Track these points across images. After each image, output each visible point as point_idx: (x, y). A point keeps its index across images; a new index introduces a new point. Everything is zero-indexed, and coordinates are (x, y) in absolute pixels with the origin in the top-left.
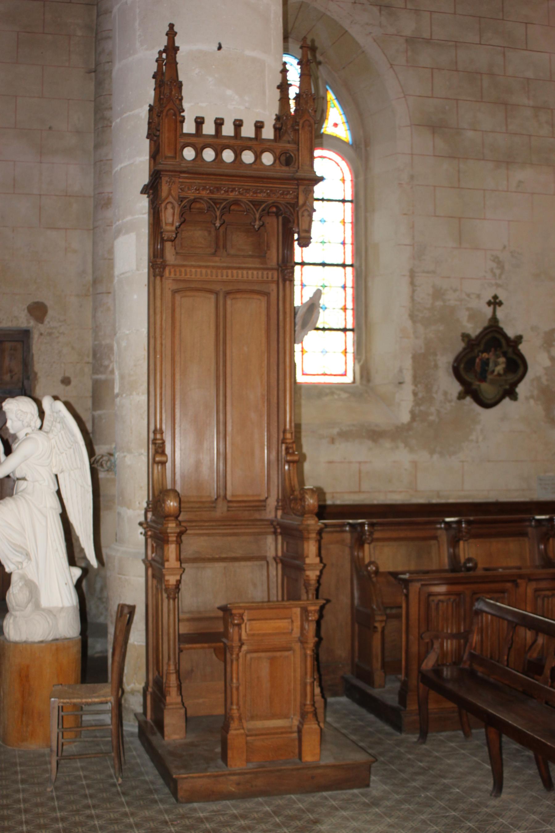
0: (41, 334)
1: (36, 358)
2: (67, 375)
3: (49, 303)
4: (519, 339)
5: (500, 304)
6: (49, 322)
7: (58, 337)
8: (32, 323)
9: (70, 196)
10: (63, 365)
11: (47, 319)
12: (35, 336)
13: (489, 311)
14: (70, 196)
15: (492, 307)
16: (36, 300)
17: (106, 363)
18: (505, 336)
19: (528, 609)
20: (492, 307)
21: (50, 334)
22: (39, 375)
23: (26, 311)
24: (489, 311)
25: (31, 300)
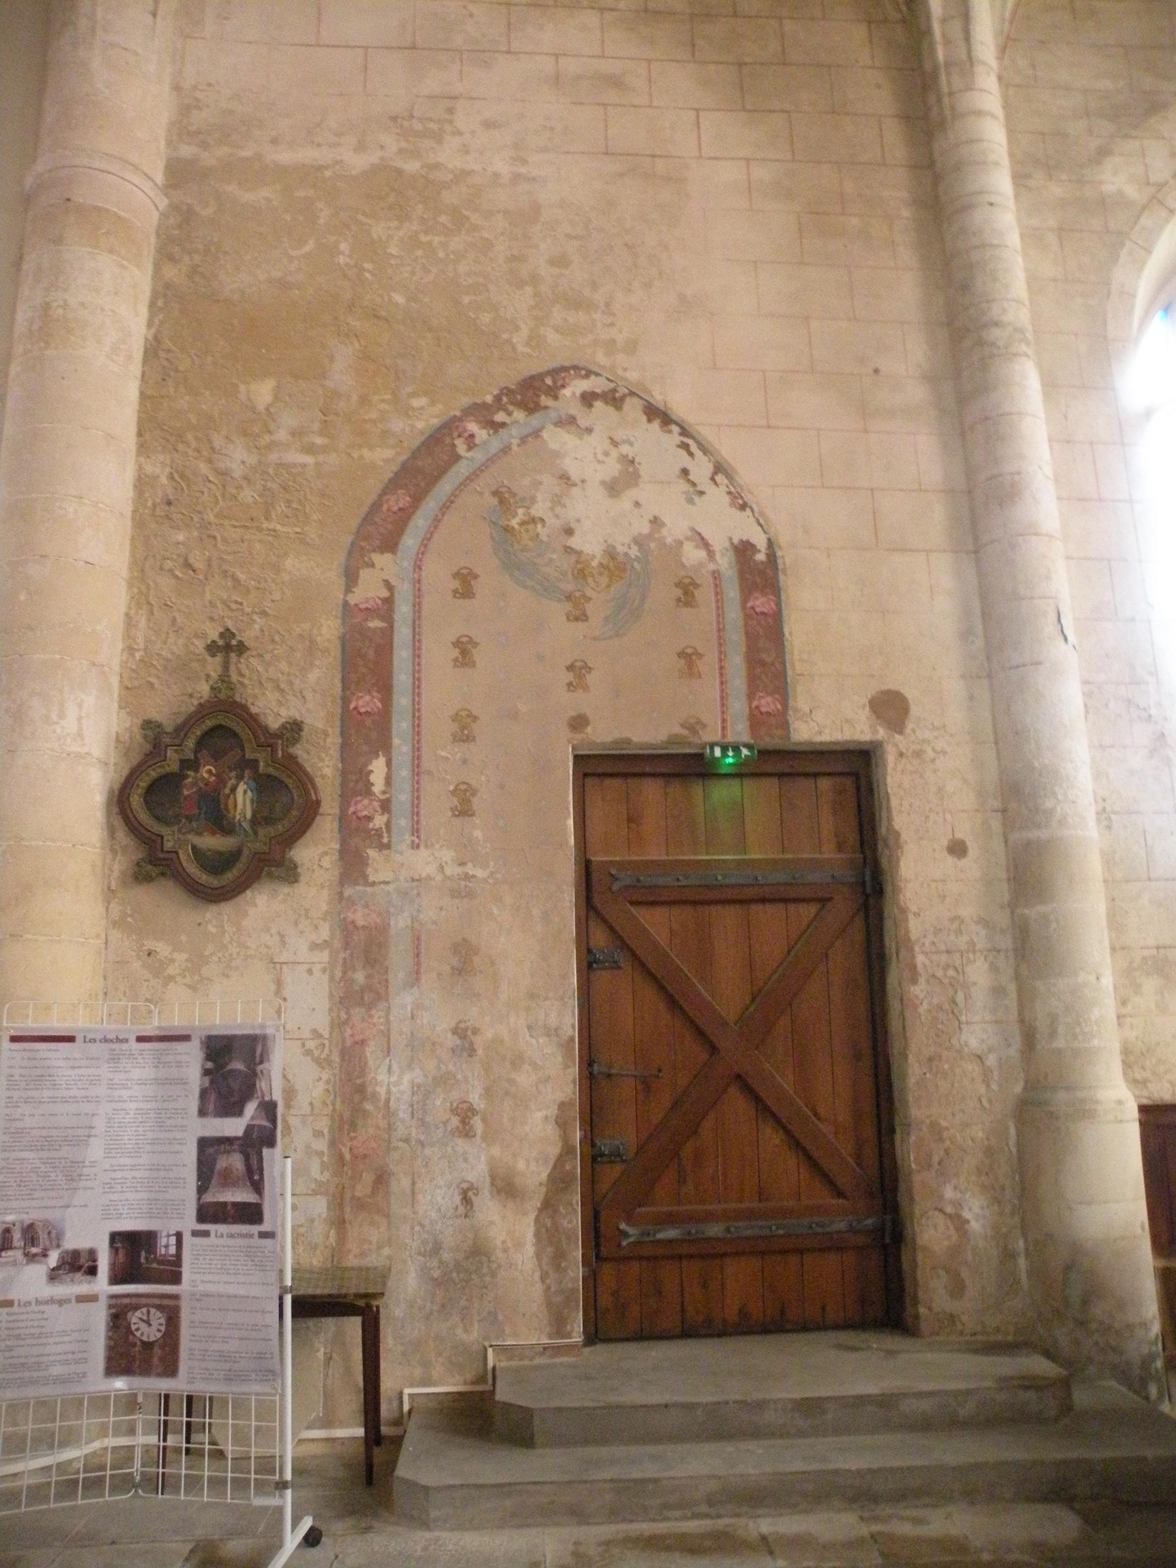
0: (901, 755)
1: (894, 802)
2: (959, 835)
3: (910, 693)
4: (295, 728)
5: (241, 648)
6: (914, 731)
7: (933, 761)
8: (881, 733)
9: (926, 491)
10: (948, 816)
11: (910, 726)
12: (891, 758)
13: (213, 666)
14: (926, 491)
15: (219, 659)
16: (885, 688)
17: (1049, 804)
18: (253, 721)
19: (435, 1375)
20: (219, 659)
21: (918, 754)
22: (904, 836)
23: (868, 708)
24: (213, 666)
25: (873, 688)
